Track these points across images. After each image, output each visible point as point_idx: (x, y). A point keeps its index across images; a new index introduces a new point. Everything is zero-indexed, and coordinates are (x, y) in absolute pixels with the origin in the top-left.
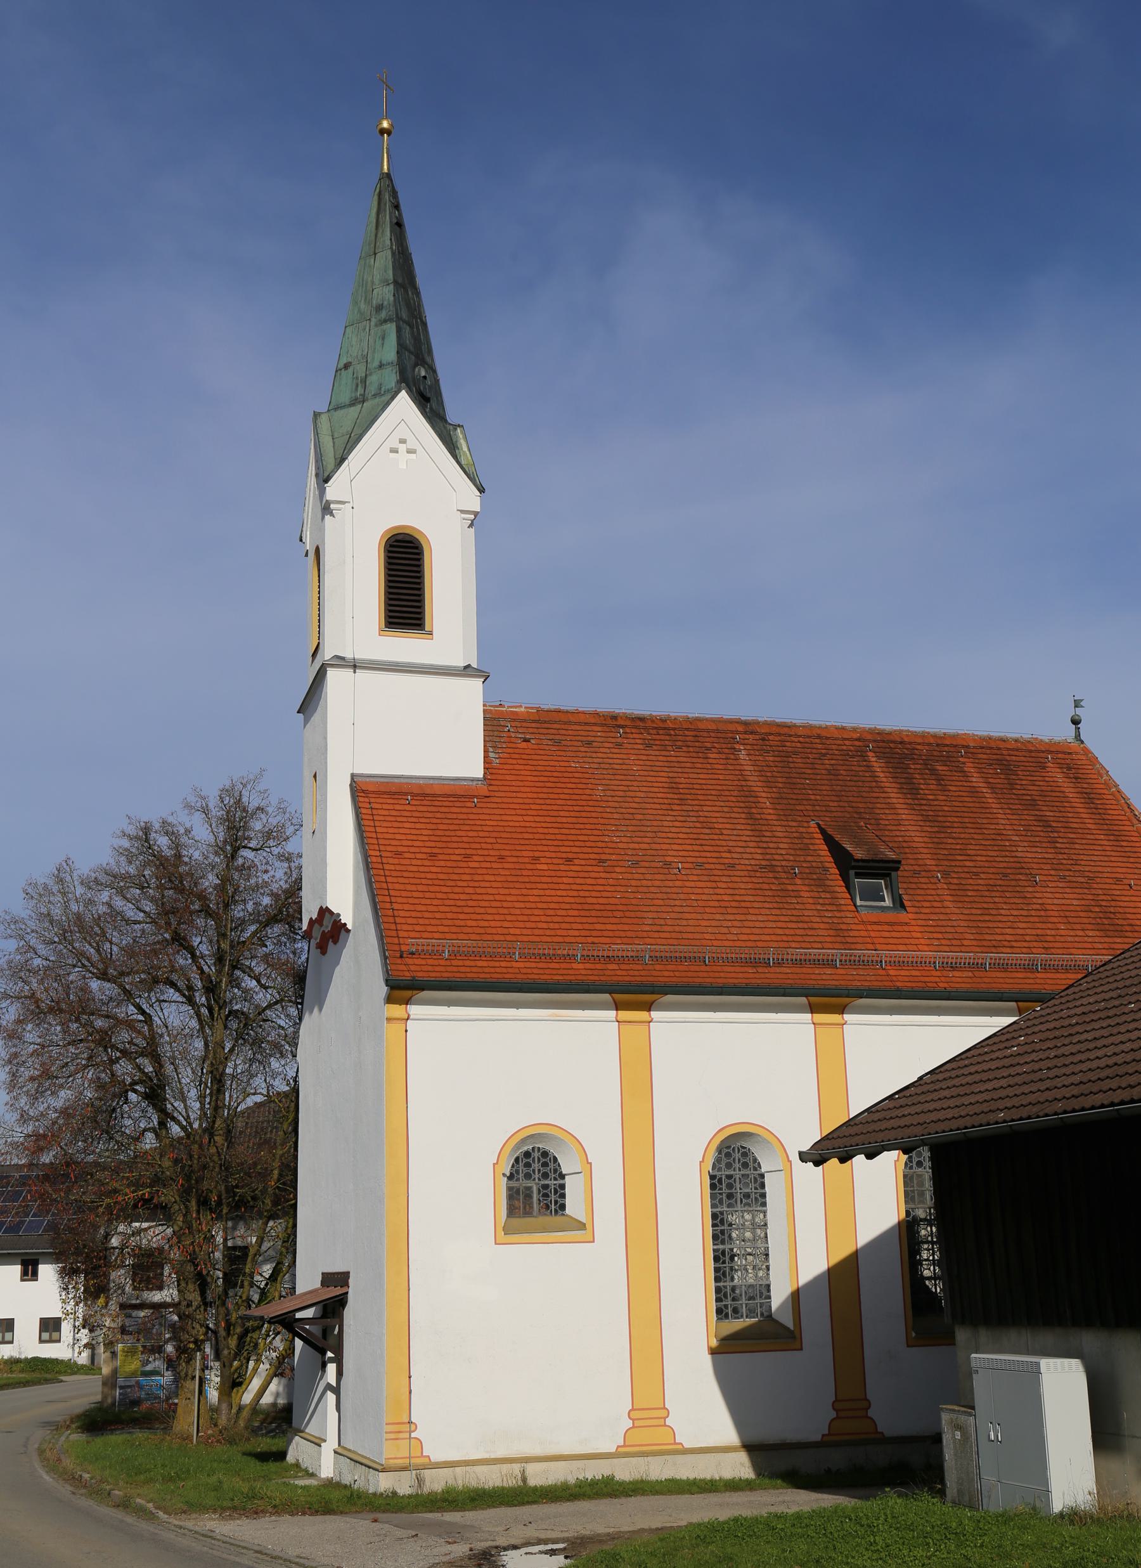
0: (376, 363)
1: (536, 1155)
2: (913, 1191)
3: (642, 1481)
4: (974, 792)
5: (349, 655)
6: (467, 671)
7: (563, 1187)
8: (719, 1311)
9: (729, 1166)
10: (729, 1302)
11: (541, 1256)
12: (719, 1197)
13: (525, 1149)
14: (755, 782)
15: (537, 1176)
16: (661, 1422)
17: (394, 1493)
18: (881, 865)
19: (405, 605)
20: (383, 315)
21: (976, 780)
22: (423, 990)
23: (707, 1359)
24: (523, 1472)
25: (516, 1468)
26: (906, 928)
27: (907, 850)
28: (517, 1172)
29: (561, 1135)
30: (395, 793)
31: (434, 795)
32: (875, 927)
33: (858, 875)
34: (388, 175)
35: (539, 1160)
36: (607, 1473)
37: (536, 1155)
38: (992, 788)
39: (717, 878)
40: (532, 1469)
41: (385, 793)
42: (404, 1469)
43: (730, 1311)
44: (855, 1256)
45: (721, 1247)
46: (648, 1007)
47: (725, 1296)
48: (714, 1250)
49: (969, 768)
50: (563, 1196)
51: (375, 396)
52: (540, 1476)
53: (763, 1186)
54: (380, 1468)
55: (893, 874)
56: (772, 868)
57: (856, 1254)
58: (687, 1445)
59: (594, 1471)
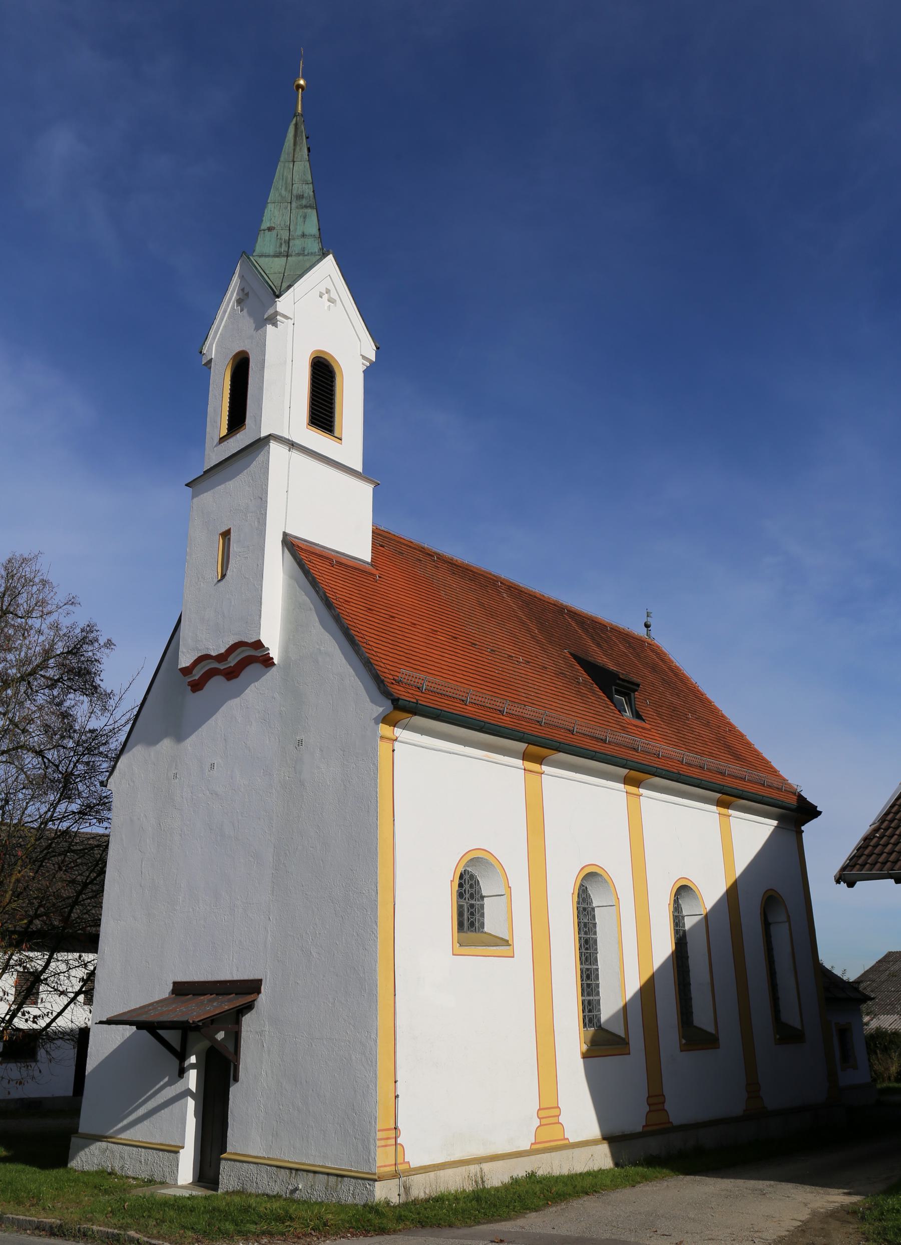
0: (299, 233)
11: (479, 966)
18: (625, 684)
19: (322, 414)
20: (304, 202)
22: (415, 714)
23: (580, 1062)
25: (474, 1169)
29: (491, 860)
51: (298, 254)
54: (376, 1177)
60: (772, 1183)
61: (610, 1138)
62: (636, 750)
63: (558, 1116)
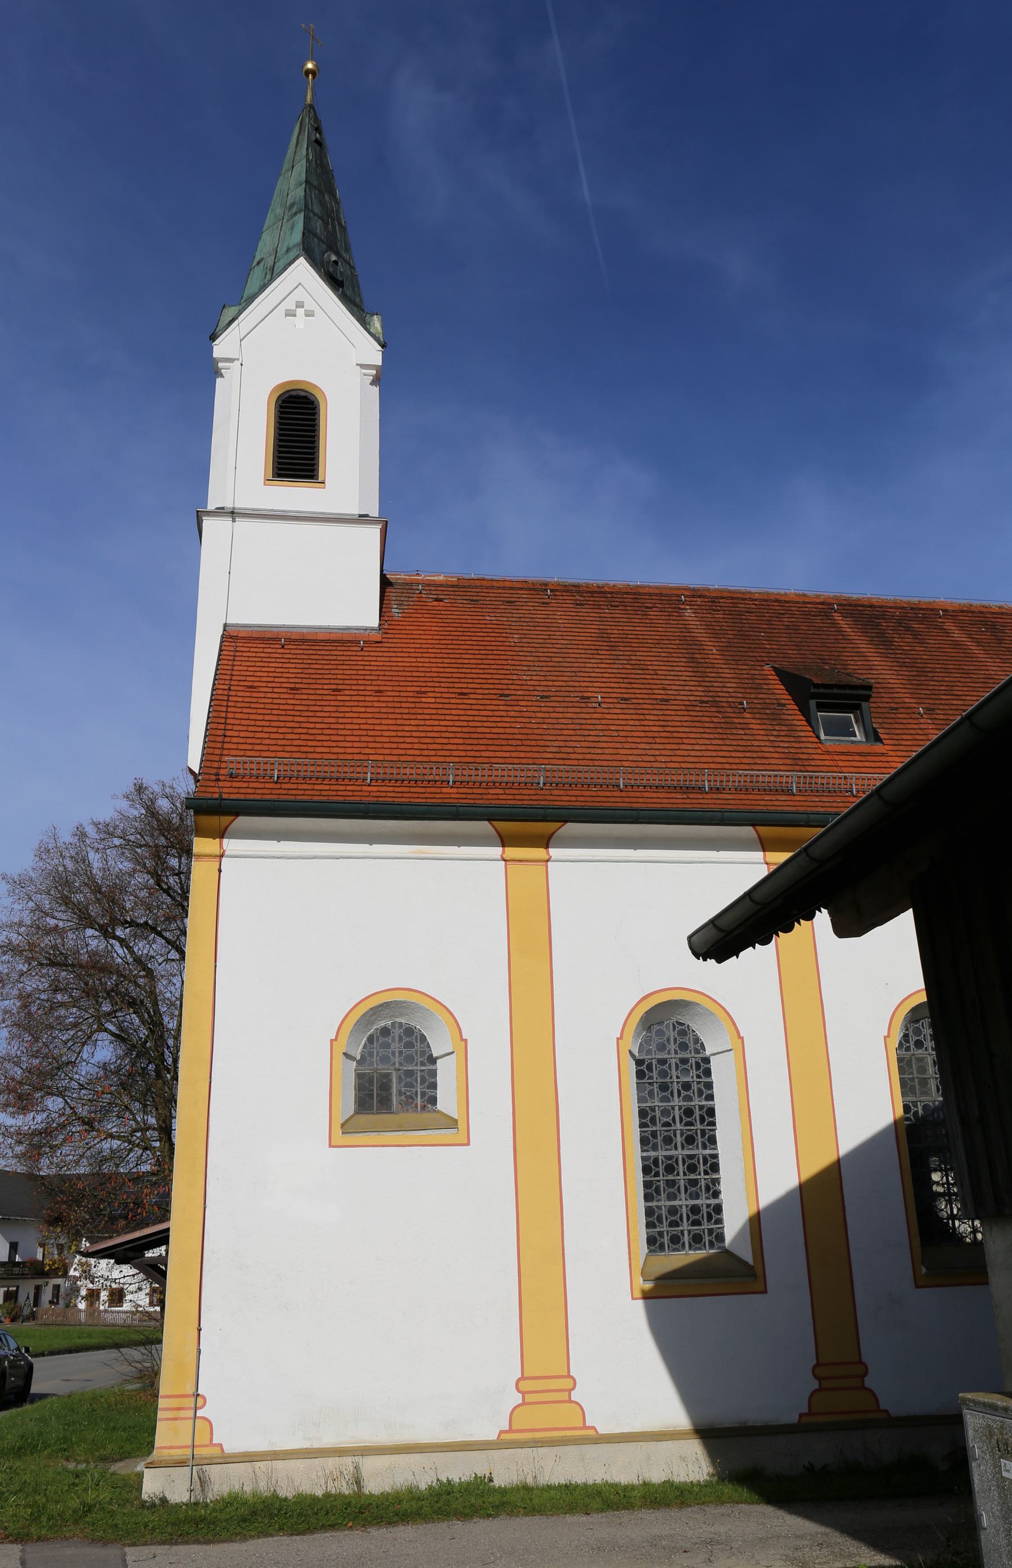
1: (397, 1032)
2: (912, 1080)
3: (526, 1488)
4: (956, 645)
5: (228, 505)
6: (363, 519)
7: (434, 1074)
8: (651, 1241)
9: (662, 1047)
10: (664, 1228)
11: (396, 1164)
12: (649, 1088)
13: (382, 1024)
14: (700, 633)
15: (397, 1060)
16: (564, 1396)
17: (164, 1501)
18: (836, 691)
20: (294, 210)
21: (957, 635)
24: (356, 1467)
25: (348, 1461)
26: (883, 759)
27: (881, 690)
28: (371, 1054)
30: (270, 639)
31: (315, 641)
32: (844, 758)
33: (821, 707)
34: (311, 106)
35: (400, 1039)
36: (482, 1471)
37: (397, 1032)
38: (979, 643)
39: (645, 712)
40: (370, 1465)
41: (257, 639)
42: (180, 1463)
43: (666, 1240)
44: (836, 1169)
45: (652, 1154)
46: (546, 842)
47: (660, 1219)
48: (643, 1159)
49: (949, 625)
50: (434, 1086)
52: (380, 1478)
53: (708, 1073)
55: (864, 705)
56: (715, 704)
57: (839, 1161)
58: (602, 1430)
59: (459, 1470)
60: (828, 1530)
61: (707, 1434)
62: (701, 789)
63: (570, 1391)
